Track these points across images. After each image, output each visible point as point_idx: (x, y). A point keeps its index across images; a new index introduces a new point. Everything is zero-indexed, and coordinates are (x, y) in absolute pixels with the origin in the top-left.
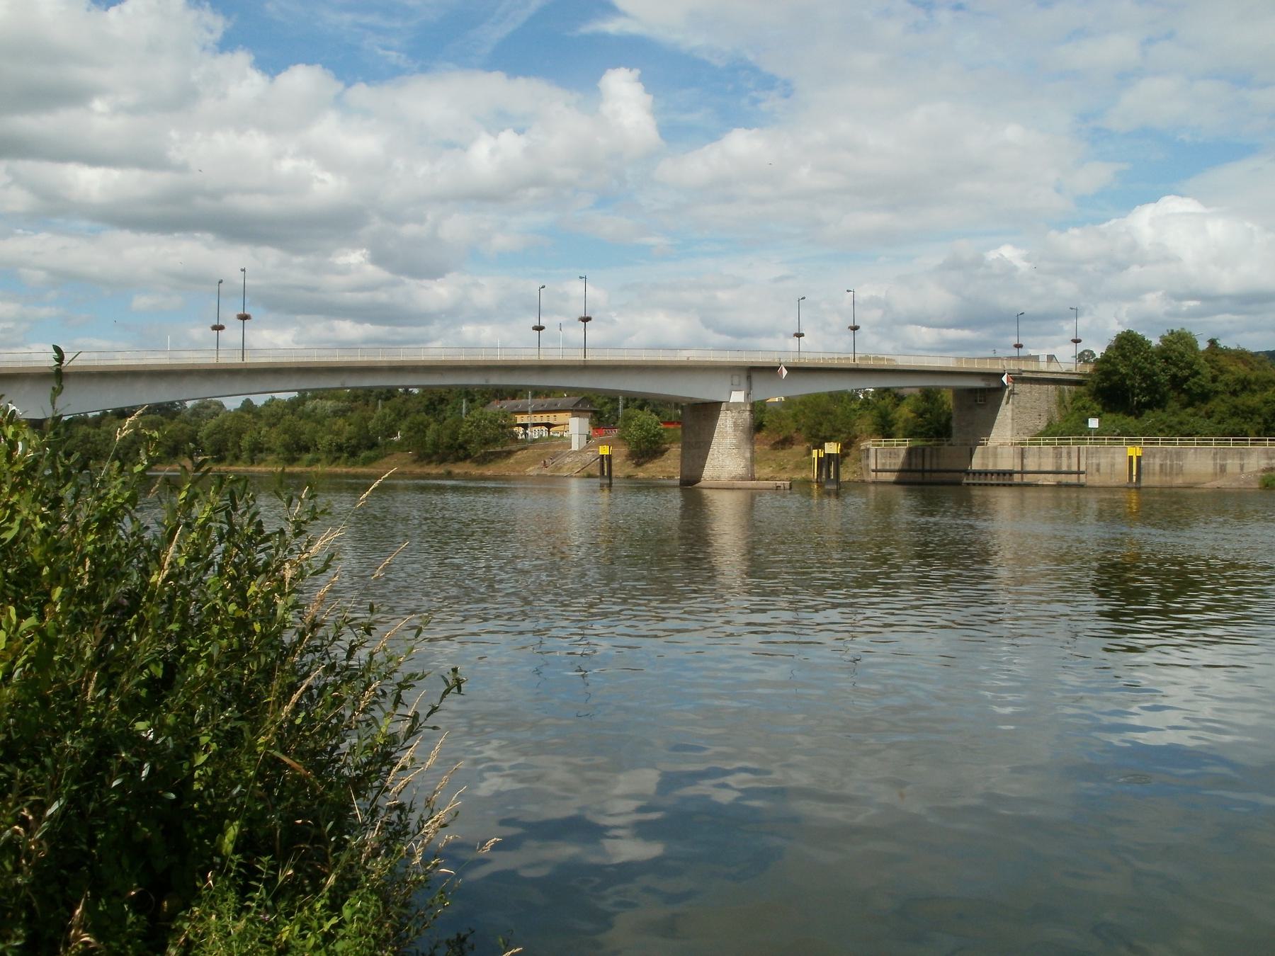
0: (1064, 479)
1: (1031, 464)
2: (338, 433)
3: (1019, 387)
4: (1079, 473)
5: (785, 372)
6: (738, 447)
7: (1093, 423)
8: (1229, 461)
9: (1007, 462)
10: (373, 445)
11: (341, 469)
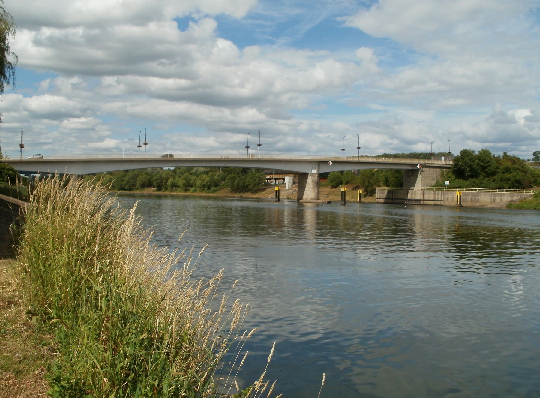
0: (436, 202)
1: (426, 197)
2: (203, 181)
3: (424, 169)
4: (441, 201)
5: (331, 163)
6: (313, 189)
7: (447, 183)
8: (497, 198)
9: (418, 196)
10: (217, 185)
11: (204, 194)
